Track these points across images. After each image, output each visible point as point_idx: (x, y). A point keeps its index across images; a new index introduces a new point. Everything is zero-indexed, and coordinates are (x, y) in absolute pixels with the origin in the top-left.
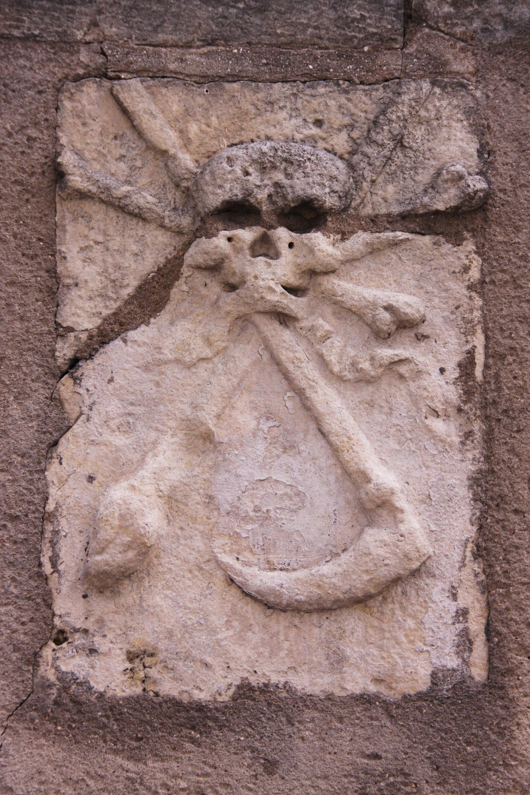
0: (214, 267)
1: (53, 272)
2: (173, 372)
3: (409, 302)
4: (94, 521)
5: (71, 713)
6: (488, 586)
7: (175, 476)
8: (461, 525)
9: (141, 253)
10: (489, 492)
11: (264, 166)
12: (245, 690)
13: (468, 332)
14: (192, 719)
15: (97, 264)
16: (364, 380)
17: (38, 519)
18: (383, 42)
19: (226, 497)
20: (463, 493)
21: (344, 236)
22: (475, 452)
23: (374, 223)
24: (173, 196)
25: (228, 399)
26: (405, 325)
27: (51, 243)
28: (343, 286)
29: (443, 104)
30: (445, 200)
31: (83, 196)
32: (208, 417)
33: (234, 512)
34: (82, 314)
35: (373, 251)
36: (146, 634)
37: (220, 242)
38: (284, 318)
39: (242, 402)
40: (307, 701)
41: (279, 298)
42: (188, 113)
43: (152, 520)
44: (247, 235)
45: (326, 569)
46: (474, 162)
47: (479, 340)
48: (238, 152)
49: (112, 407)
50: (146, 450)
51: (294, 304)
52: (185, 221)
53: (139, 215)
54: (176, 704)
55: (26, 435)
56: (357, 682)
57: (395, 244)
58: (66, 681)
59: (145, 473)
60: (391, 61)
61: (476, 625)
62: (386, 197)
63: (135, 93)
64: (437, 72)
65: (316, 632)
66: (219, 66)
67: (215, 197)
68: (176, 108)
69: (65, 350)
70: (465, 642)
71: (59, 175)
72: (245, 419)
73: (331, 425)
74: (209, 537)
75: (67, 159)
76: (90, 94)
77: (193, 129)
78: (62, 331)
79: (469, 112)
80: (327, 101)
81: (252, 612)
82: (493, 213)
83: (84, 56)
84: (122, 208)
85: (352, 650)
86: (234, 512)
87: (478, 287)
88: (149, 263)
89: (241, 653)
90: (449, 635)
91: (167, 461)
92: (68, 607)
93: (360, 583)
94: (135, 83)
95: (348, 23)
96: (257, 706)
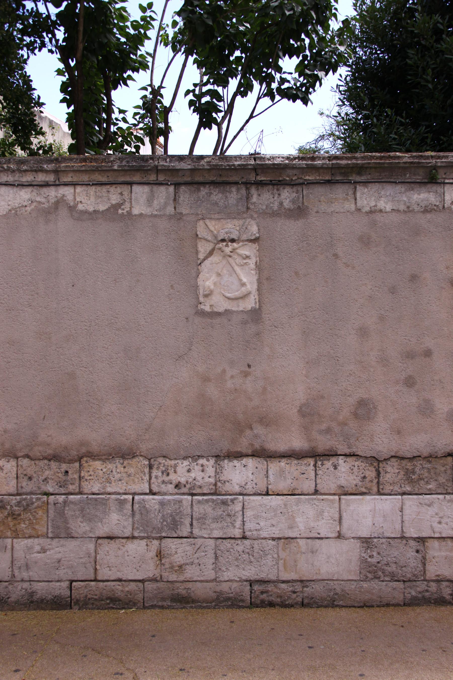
0: (220, 249)
1: (197, 250)
2: (215, 265)
3: (247, 253)
4: (204, 288)
5: (202, 314)
6: (259, 295)
7: (215, 280)
8: (255, 286)
9: (209, 247)
10: (259, 282)
11: (227, 233)
12: (226, 310)
13: (256, 258)
14: (219, 314)
15: (203, 248)
16: (242, 265)
17: (196, 287)
18: (244, 213)
19: (222, 283)
20: (256, 282)
21: (239, 243)
22: (257, 275)
23: (243, 241)
24: (213, 238)
25: (222, 269)
26: (248, 257)
27: (196, 246)
28: (238, 251)
29: (253, 222)
30: (253, 238)
31: (201, 238)
32: (219, 271)
33: (224, 285)
34: (201, 256)
35: (243, 245)
36: (212, 303)
37: (220, 245)
38: (230, 256)
39: (224, 269)
40: (234, 311)
41: (229, 253)
42: (215, 225)
43: (212, 287)
44: (224, 244)
45: (237, 293)
46: (257, 231)
47: (258, 259)
48: (222, 231)
49: (206, 270)
50: (211, 276)
51: (231, 254)
52: (215, 242)
53: (209, 241)
54: (217, 312)
55: (194, 275)
56: (241, 309)
57: (246, 244)
58: (202, 309)
59: (211, 280)
60: (245, 215)
61: (257, 300)
62: (244, 237)
63: (207, 222)
64: (252, 217)
65: (235, 302)
66: (220, 217)
67: (220, 238)
68: (214, 224)
69: (199, 262)
70: (256, 303)
71: (197, 235)
72: (225, 272)
73: (237, 272)
74: (220, 289)
75: (198, 233)
76: (201, 223)
77: (216, 227)
78: (198, 259)
79: (257, 223)
80: (236, 222)
81: (226, 299)
82: (260, 239)
83: (200, 216)
84: (206, 240)
85: (240, 304)
86: (224, 285)
87: (258, 251)
88: (210, 248)
89: (225, 305)
90: (253, 302)
91: (214, 278)
92: (201, 299)
93: (241, 295)
94: (208, 220)
95: (238, 210)
96: (227, 312)
